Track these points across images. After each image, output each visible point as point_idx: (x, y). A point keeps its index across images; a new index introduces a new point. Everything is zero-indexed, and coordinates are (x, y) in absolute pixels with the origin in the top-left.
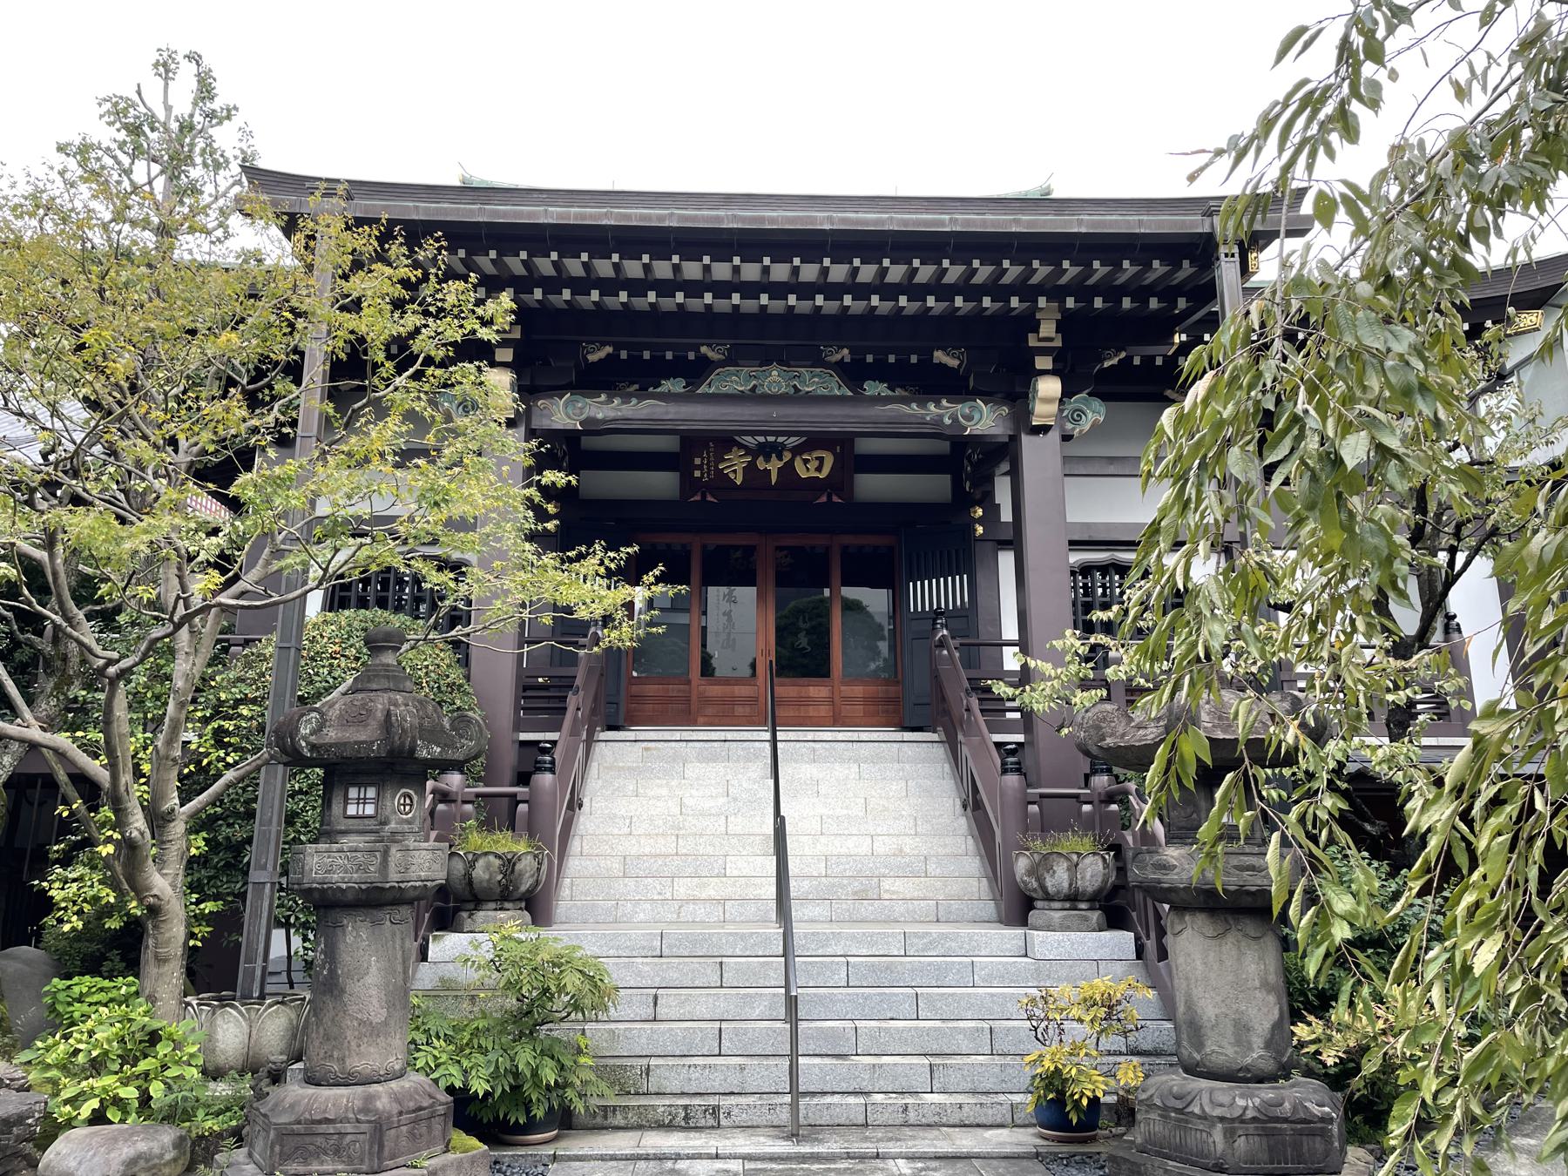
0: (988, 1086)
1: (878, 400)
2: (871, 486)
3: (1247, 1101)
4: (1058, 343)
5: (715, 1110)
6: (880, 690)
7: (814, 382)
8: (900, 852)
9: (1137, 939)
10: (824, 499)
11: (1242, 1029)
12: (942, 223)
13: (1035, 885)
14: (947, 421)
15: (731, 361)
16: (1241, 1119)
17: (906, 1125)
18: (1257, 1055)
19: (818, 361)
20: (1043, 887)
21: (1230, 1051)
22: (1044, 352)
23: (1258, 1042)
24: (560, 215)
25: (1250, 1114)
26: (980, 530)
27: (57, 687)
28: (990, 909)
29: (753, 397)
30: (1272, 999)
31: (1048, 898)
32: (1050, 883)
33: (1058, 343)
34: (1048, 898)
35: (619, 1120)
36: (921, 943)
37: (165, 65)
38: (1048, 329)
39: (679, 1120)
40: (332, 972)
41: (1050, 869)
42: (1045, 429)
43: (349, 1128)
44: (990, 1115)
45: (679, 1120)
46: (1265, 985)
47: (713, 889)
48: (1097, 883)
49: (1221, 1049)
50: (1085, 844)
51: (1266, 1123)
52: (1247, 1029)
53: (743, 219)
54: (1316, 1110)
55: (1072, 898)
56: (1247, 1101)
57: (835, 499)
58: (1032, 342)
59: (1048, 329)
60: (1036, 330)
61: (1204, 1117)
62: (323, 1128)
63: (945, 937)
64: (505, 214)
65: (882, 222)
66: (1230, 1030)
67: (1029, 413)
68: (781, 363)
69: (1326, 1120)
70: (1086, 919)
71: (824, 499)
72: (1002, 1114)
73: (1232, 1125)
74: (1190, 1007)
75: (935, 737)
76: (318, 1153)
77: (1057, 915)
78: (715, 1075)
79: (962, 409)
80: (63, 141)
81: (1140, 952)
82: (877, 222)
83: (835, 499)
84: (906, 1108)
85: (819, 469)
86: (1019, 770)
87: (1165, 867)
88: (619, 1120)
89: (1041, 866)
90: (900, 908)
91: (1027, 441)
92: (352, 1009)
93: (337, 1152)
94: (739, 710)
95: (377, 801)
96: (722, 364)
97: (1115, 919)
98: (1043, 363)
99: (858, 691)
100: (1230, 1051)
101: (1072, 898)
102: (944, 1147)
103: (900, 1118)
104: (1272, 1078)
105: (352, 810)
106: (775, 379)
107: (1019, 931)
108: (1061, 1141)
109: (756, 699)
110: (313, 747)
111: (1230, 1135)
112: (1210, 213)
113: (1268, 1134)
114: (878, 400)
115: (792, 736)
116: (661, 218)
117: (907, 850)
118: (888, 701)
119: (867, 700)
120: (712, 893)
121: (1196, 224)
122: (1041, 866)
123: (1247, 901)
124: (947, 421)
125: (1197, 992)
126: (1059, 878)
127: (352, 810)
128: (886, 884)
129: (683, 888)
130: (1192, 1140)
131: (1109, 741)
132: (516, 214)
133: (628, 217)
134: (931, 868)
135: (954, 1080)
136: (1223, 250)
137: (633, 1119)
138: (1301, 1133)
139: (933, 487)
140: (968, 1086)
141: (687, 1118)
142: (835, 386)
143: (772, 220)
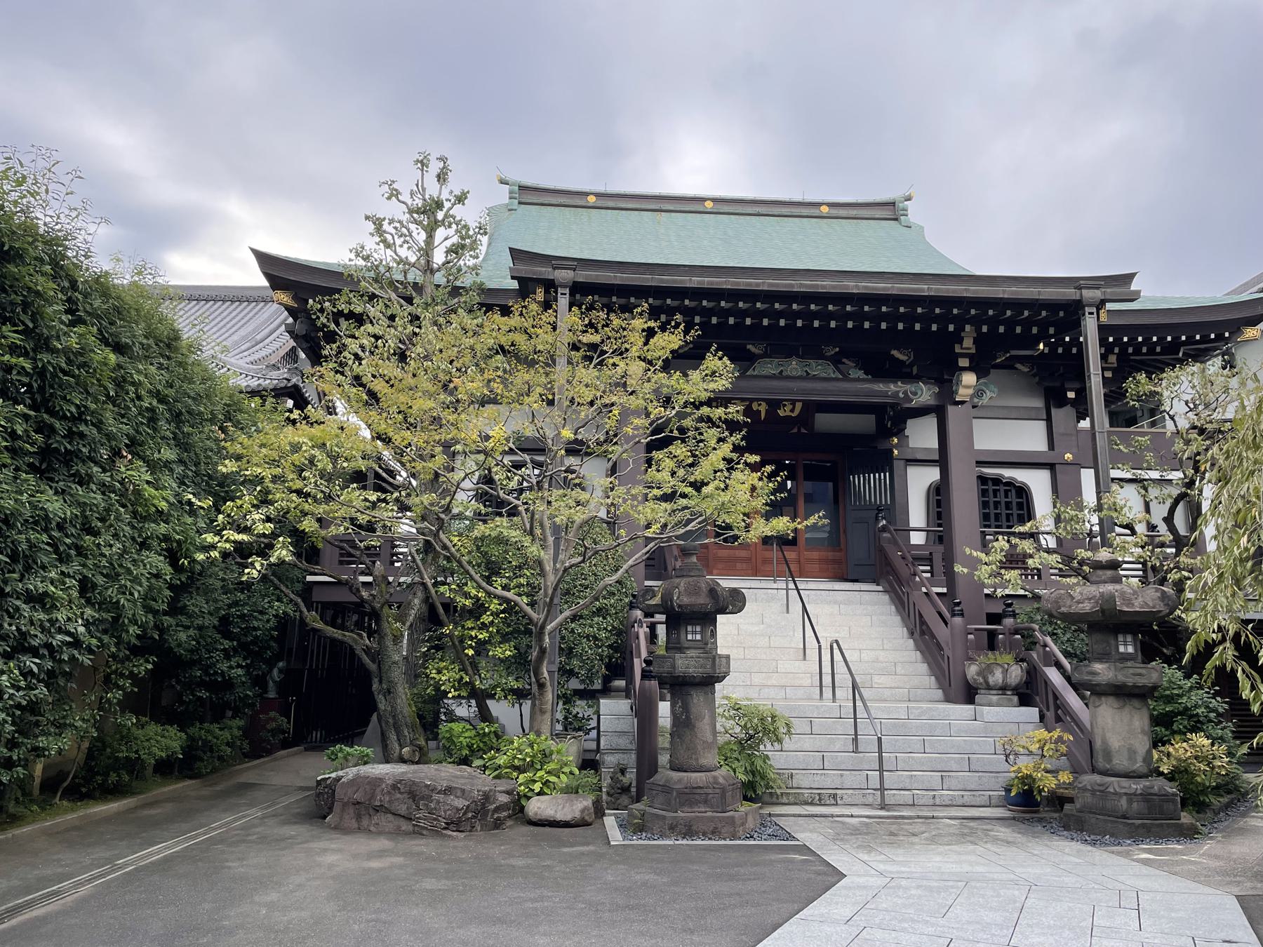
0: (973, 787)
1: (858, 380)
2: (824, 421)
3: (1137, 786)
4: (973, 351)
5: (835, 796)
6: (830, 555)
7: (818, 368)
8: (877, 660)
9: (1040, 711)
10: (795, 430)
11: (1132, 752)
12: (923, 290)
13: (981, 680)
14: (901, 395)
15: (765, 355)
16: (1134, 794)
17: (934, 805)
18: (1139, 765)
19: (821, 356)
20: (987, 682)
21: (1126, 763)
22: (964, 355)
23: (1140, 759)
24: (699, 282)
25: (1139, 792)
26: (896, 452)
27: (433, 559)
28: (939, 694)
29: (780, 376)
30: (1146, 738)
31: (989, 688)
32: (991, 680)
33: (973, 351)
34: (989, 688)
35: (785, 800)
36: (917, 712)
37: (422, 162)
38: (968, 343)
39: (816, 800)
40: (688, 717)
41: (992, 672)
42: (962, 403)
43: (710, 791)
44: (978, 801)
45: (816, 800)
46: (1143, 732)
47: (774, 681)
48: (1017, 681)
49: (1121, 762)
50: (1008, 658)
51: (1146, 796)
52: (1135, 752)
53: (806, 286)
54: (1170, 790)
55: (1003, 689)
56: (1137, 786)
57: (803, 431)
58: (958, 350)
59: (968, 343)
60: (961, 342)
61: (1116, 793)
62: (699, 791)
63: (930, 709)
64: (668, 281)
65: (888, 289)
66: (1126, 753)
67: (953, 393)
68: (798, 356)
69: (1174, 795)
70: (1010, 700)
71: (795, 430)
72: (984, 800)
73: (1131, 796)
74: (1104, 742)
75: (880, 588)
76: (697, 803)
77: (995, 698)
78: (828, 780)
79: (909, 387)
80: (369, 214)
81: (1042, 717)
82: (884, 289)
83: (803, 431)
84: (934, 797)
85: (792, 411)
86: (962, 615)
87: (1094, 673)
88: (785, 800)
89: (986, 671)
90: (887, 693)
91: (951, 409)
92: (699, 735)
93: (706, 802)
94: (739, 565)
95: (702, 633)
96: (761, 356)
97: (1025, 701)
98: (964, 362)
99: (815, 555)
100: (1126, 763)
101: (1003, 689)
102: (966, 815)
103: (931, 802)
104: (1147, 777)
105: (690, 637)
106: (794, 366)
107: (972, 707)
108: (1023, 812)
109: (750, 559)
110: (680, 606)
111: (1130, 802)
112: (1080, 288)
113: (1147, 801)
114: (858, 380)
115: (812, 585)
116: (758, 285)
117: (881, 659)
118: (834, 561)
119: (821, 561)
120: (775, 682)
121: (1070, 293)
122: (986, 671)
123: (1137, 691)
124: (901, 395)
125: (1108, 735)
126: (997, 677)
127: (690, 637)
128: (876, 679)
129: (757, 679)
130: (1109, 805)
131: (1063, 609)
132: (675, 281)
133: (738, 284)
134: (899, 670)
135: (953, 783)
136: (1087, 310)
137: (792, 799)
138: (1163, 801)
139: (863, 423)
140: (961, 787)
141: (820, 800)
142: (831, 372)
143: (823, 287)
